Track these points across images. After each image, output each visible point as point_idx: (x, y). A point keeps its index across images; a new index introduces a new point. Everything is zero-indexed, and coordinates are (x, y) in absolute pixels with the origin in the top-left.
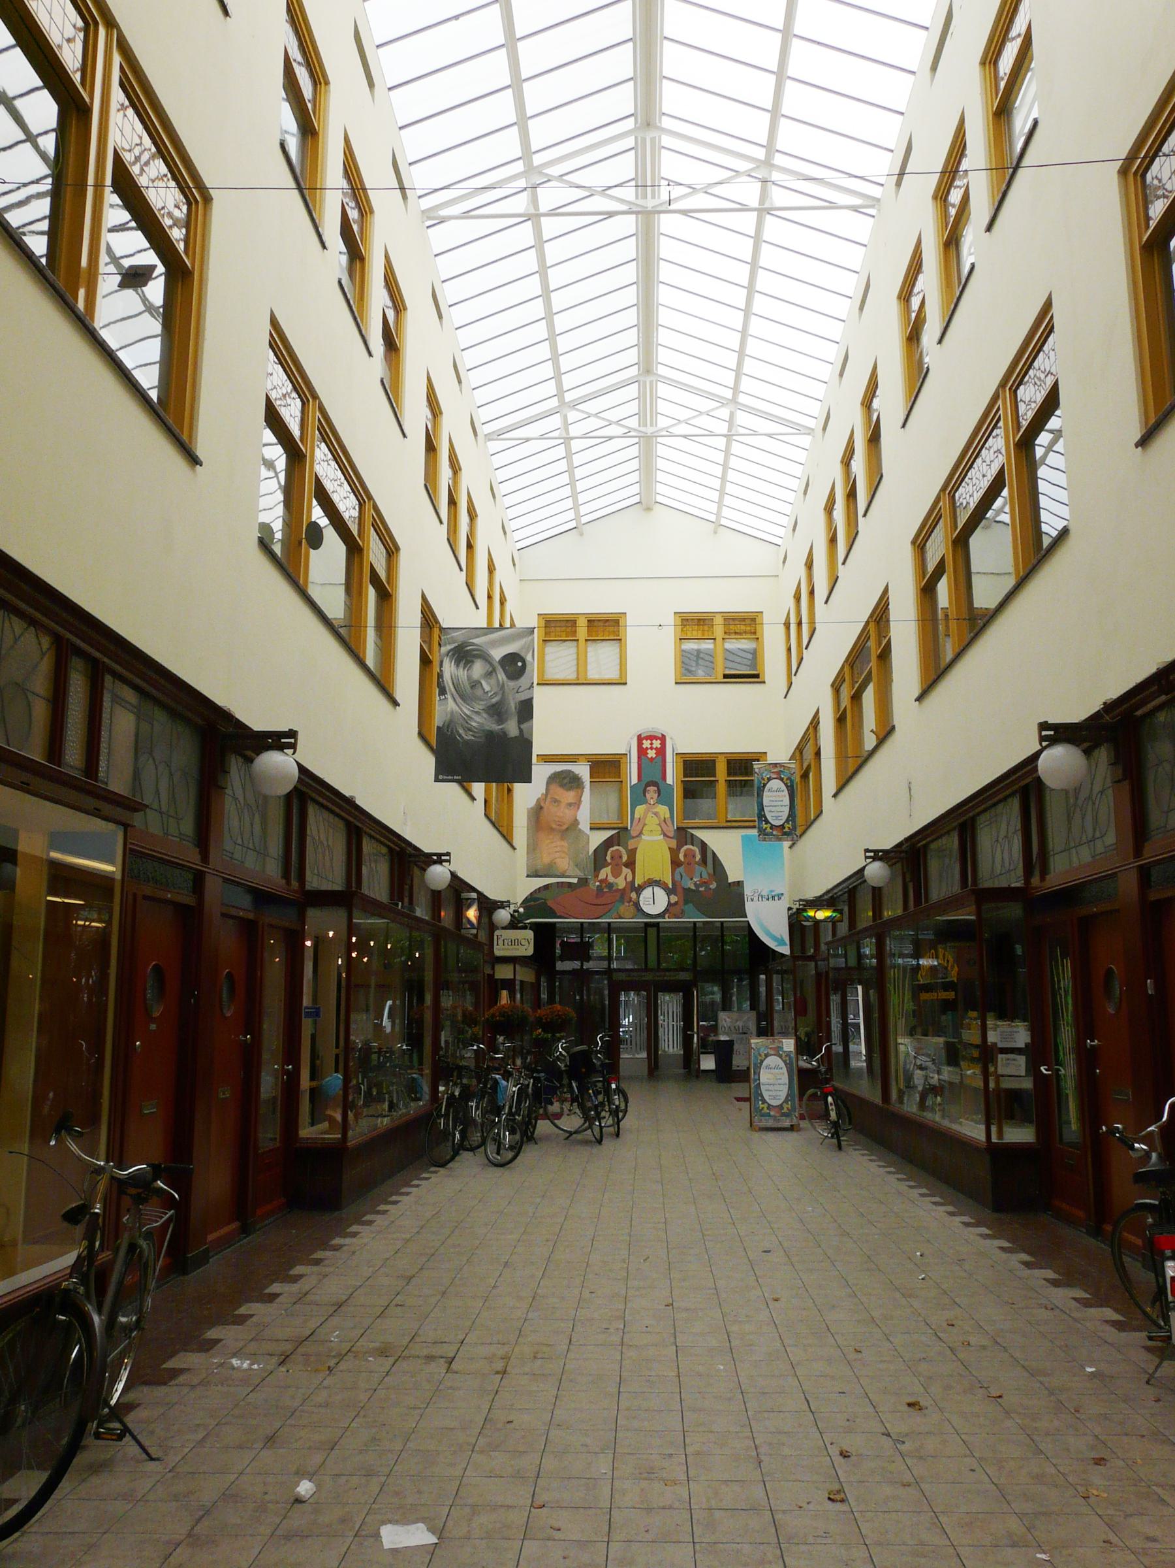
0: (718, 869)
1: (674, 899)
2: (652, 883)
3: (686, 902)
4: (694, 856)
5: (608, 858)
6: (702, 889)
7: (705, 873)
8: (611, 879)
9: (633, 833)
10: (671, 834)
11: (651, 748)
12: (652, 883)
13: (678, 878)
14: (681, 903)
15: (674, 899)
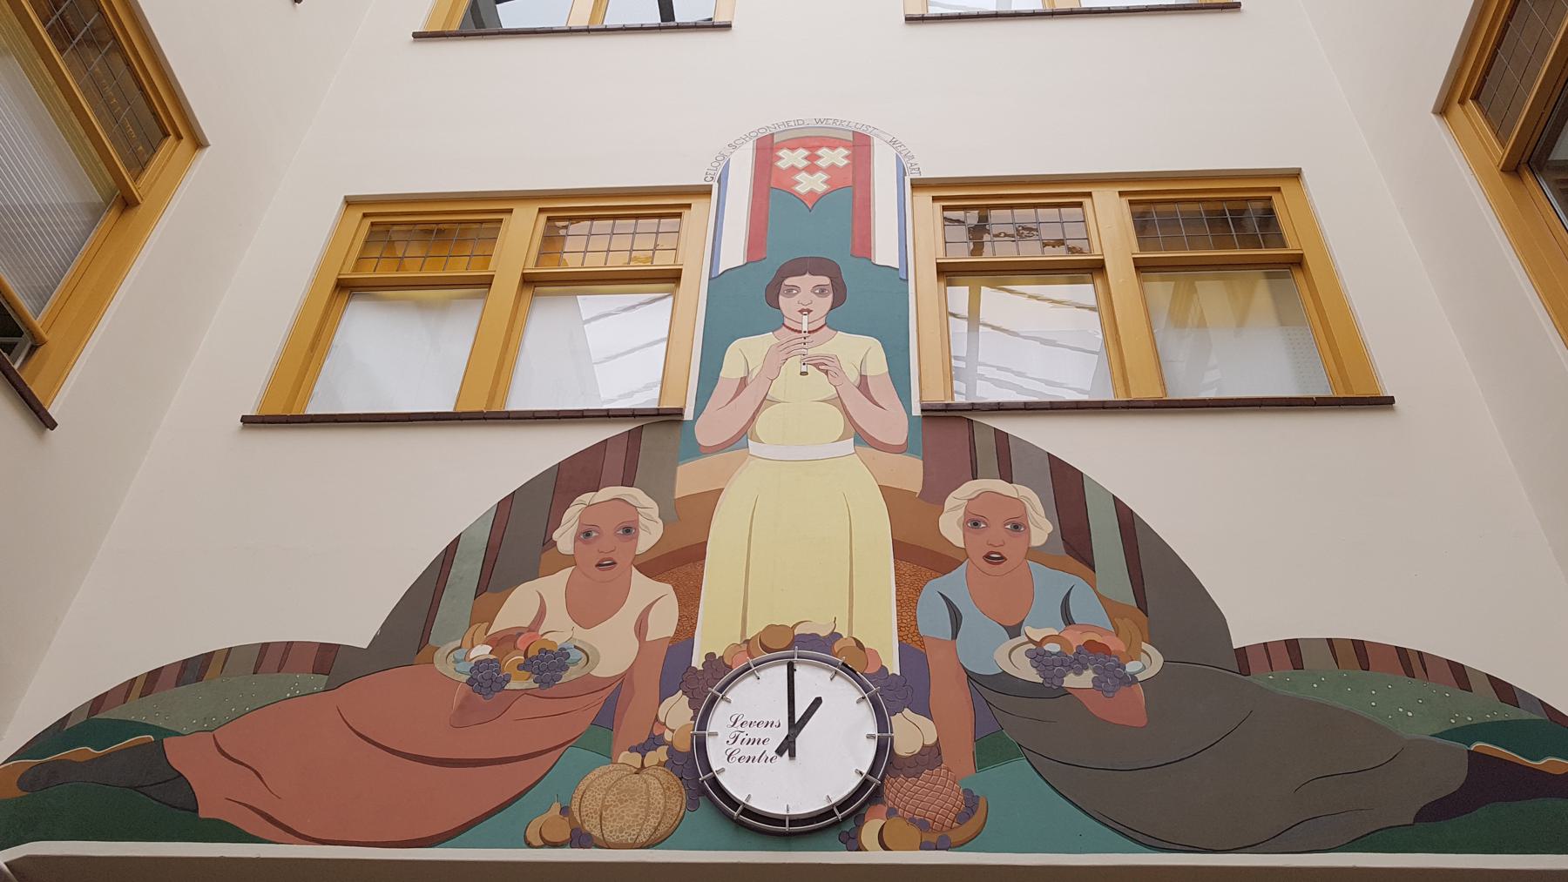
0: (1158, 582)
1: (913, 733)
2: (793, 647)
5: (564, 538)
8: (560, 630)
9: (705, 434)
10: (899, 435)
12: (793, 647)
13: (932, 621)
14: (960, 755)
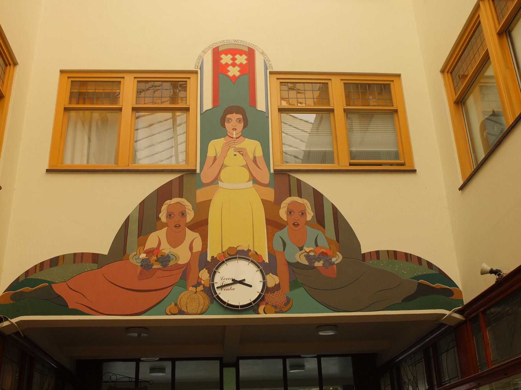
1: (273, 280)
3: (294, 285)
4: (303, 213)
6: (319, 264)
7: (325, 238)
8: (166, 249)
9: (205, 178)
10: (265, 179)
11: (234, 65)
13: (278, 246)
14: (285, 286)
15: (273, 280)
